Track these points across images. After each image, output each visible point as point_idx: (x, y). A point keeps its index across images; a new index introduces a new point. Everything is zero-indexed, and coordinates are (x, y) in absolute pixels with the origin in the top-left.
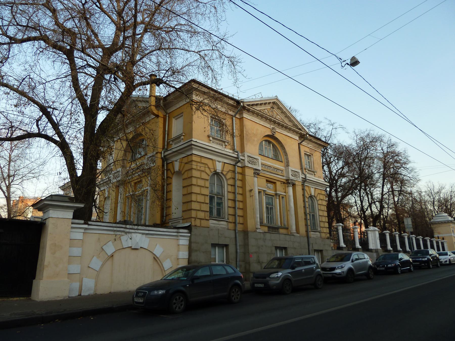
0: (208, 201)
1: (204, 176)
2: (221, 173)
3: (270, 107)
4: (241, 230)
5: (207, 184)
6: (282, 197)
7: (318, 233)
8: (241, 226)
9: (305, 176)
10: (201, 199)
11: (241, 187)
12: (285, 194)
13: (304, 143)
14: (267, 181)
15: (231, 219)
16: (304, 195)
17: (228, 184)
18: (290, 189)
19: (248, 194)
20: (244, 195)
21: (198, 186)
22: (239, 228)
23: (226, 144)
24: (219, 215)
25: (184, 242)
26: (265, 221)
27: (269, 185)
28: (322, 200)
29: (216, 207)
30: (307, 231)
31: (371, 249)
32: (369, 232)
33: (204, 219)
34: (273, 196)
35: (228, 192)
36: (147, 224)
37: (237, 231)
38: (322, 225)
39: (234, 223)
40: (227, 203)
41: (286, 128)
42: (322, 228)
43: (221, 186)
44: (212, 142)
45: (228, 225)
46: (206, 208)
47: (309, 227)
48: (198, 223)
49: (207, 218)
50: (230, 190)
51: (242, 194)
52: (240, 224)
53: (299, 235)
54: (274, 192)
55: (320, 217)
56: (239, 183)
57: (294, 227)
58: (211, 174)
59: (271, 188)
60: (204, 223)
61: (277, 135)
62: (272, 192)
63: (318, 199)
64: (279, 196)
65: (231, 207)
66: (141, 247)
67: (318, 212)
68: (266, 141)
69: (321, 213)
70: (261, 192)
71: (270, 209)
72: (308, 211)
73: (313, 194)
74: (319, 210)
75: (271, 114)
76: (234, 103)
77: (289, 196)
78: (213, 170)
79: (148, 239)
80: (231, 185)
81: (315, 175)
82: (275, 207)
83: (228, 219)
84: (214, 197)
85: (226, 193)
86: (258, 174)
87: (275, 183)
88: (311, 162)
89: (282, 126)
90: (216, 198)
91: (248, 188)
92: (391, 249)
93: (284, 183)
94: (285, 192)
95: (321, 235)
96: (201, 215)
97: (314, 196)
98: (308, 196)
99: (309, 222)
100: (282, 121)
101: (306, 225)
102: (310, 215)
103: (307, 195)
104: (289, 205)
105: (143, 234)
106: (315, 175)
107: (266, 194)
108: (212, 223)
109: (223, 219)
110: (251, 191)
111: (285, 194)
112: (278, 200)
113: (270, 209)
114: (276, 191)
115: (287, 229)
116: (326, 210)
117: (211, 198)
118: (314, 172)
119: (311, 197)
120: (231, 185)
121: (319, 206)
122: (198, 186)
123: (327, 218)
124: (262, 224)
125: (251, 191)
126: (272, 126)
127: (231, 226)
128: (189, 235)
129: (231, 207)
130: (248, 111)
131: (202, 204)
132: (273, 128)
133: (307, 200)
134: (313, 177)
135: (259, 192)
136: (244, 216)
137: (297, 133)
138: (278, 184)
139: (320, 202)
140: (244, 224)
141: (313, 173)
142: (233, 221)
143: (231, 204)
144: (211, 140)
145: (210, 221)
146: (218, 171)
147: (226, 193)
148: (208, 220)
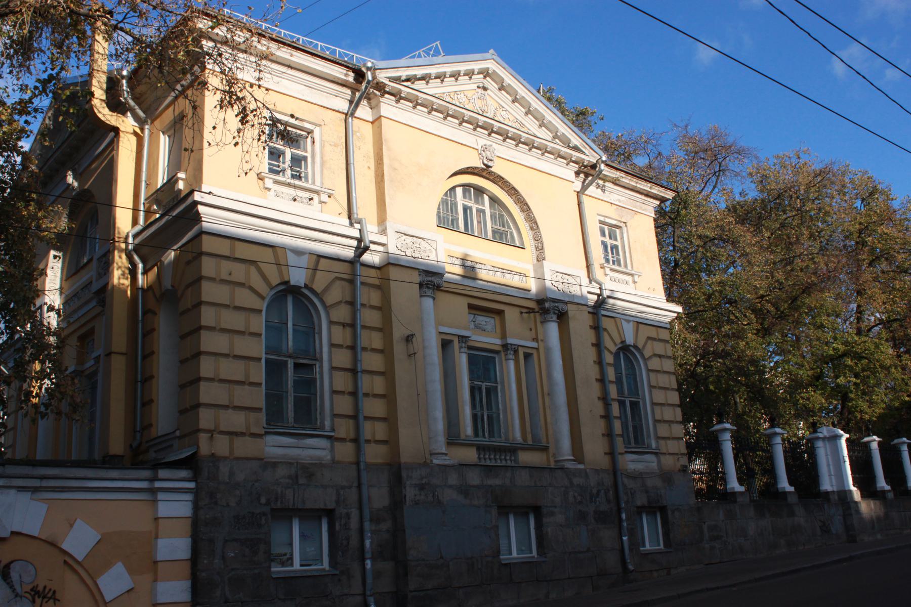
0: (259, 373)
1: (245, 298)
2: (306, 286)
3: (475, 86)
4: (380, 461)
5: (259, 324)
6: (527, 356)
7: (652, 458)
8: (382, 449)
9: (601, 289)
10: (231, 370)
11: (380, 330)
12: (534, 345)
13: (592, 190)
14: (471, 307)
15: (344, 429)
16: (598, 345)
17: (331, 323)
18: (553, 329)
19: (399, 349)
20: (386, 352)
21: (223, 330)
22: (374, 454)
23: (324, 197)
24: (306, 415)
25: (176, 507)
26: (468, 429)
27: (481, 319)
28: (660, 356)
29: (291, 391)
30: (612, 453)
31: (827, 493)
32: (819, 444)
33: (243, 434)
34: (497, 352)
35: (334, 392)
36: (39, 456)
37: (362, 466)
38: (663, 430)
39: (350, 394)
40: (330, 381)
41: (531, 145)
42: (662, 442)
43: (309, 331)
44: (272, 193)
45: (332, 449)
46: (258, 397)
47: (619, 442)
48: (221, 446)
49: (254, 430)
50: (337, 340)
51: (381, 351)
52: (378, 442)
53: (581, 466)
54: (499, 342)
55: (657, 410)
56: (370, 317)
57: (566, 444)
58: (268, 294)
59: (489, 328)
60: (245, 447)
61: (498, 168)
62: (491, 340)
63: (647, 354)
64: (516, 352)
65: (339, 346)
66: (13, 533)
67: (650, 392)
68: (466, 187)
69: (659, 397)
70: (451, 341)
71: (485, 393)
72: (613, 391)
73: (630, 340)
74: (651, 387)
75: (478, 105)
76: (346, 75)
77: (548, 350)
78: (618, 341)
79: (44, 507)
80: (344, 325)
81: (635, 282)
82: (503, 383)
83: (333, 430)
84: (286, 362)
85: (325, 349)
86: (438, 288)
87: (500, 313)
88: (623, 247)
89: (518, 141)
90: (290, 364)
91: (398, 332)
92: (888, 488)
93: (530, 311)
94: (535, 339)
95: (659, 462)
96: (236, 421)
97: (635, 347)
98: (614, 349)
99: (617, 426)
100: (517, 125)
101: (609, 435)
102: (622, 403)
103: (607, 342)
104: (550, 376)
105: (21, 489)
106: (635, 282)
107: (470, 348)
108: (276, 447)
109: (315, 429)
110: (409, 339)
111: (534, 345)
112: (512, 364)
113: (485, 393)
114: (504, 336)
115: (545, 449)
116: (118, 209)
117: (274, 369)
118: (632, 275)
119: (625, 348)
120: (344, 325)
121: (652, 375)
122: (223, 330)
123: (679, 411)
124: (453, 439)
125: (409, 339)
126: (482, 142)
127: (345, 451)
128: (192, 485)
129: (342, 393)
130: (398, 96)
131: (237, 388)
132: (485, 148)
133: (609, 358)
134: (630, 288)
135: (446, 344)
136: (390, 420)
137: (570, 160)
138: (511, 315)
139: (654, 364)
140: (391, 441)
141: (629, 278)
142: (350, 389)
143: (342, 381)
144: (269, 189)
145: (270, 439)
146: (628, 343)
147: (325, 349)
148: (260, 436)
